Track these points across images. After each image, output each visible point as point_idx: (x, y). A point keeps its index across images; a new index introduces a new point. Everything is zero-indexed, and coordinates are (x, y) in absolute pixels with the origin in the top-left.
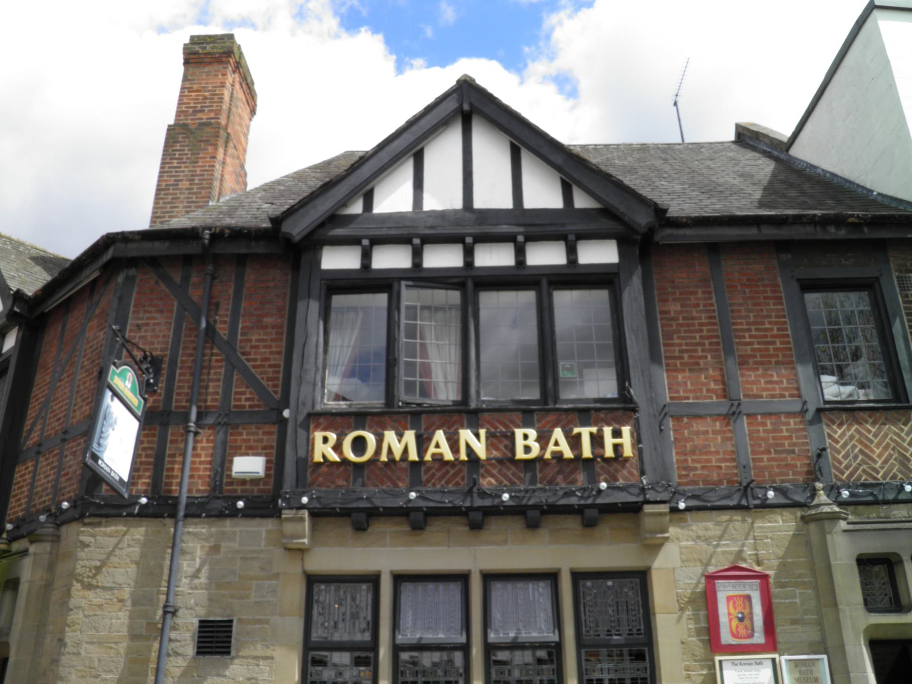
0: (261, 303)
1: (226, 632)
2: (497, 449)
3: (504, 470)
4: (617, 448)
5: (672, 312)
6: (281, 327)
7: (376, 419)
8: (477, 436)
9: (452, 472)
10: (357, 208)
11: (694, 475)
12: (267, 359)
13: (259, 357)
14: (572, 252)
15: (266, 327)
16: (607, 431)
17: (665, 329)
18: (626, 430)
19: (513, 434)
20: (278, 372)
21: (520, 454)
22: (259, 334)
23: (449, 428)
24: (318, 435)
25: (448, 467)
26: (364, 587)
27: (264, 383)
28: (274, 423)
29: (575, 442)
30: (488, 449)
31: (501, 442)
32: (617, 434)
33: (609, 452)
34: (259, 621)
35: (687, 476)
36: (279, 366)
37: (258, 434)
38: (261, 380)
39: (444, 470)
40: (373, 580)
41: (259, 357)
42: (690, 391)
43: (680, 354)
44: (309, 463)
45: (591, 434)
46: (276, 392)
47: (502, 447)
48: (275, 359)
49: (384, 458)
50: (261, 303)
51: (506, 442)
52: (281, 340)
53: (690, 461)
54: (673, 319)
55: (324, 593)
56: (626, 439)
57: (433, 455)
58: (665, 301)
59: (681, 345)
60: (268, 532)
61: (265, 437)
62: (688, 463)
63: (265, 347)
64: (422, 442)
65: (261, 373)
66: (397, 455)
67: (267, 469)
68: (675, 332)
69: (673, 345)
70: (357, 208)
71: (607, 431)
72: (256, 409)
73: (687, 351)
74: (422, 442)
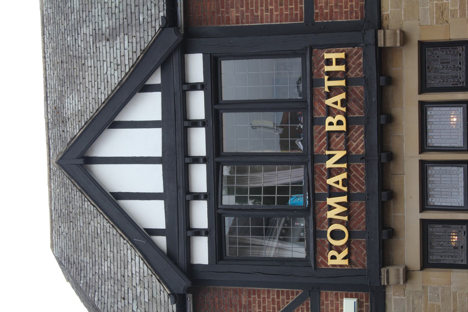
0: (231, 307)
1: (251, 179)
2: (338, 143)
3: (354, 138)
4: (339, 62)
5: (237, 15)
6: (249, 291)
7: (318, 224)
8: (330, 156)
9: (354, 173)
10: (162, 241)
11: (356, 8)
12: (273, 299)
13: (272, 306)
14: (194, 87)
15: (250, 302)
16: (327, 68)
17: (250, 20)
18: (327, 56)
19: (329, 132)
20: (283, 291)
21: (343, 128)
22: (255, 306)
23: (324, 174)
24: (331, 262)
25: (351, 176)
26: (430, 230)
27: (291, 301)
28: (320, 293)
29: (333, 91)
30: (340, 150)
31: (334, 140)
32: (329, 62)
33: (342, 68)
34: (455, 299)
35: (356, 12)
36: (278, 292)
37: (328, 304)
38: (289, 303)
39: (353, 178)
40: (424, 224)
41: (272, 306)
42: (296, 6)
43: (269, 11)
44: (349, 268)
45: (329, 80)
46: (297, 293)
47: (337, 140)
48: (273, 295)
49: (346, 218)
50: (231, 307)
51: (334, 136)
52: (260, 290)
53: (346, 10)
54: (243, 15)
55: (433, 258)
56: (333, 56)
57: (343, 185)
58: (228, 19)
59: (262, 10)
60: (394, 295)
61: (330, 299)
62: (348, 11)
63: (264, 302)
64: (332, 192)
65: (283, 304)
66: (343, 209)
67: (351, 297)
68: (252, 14)
69: (262, 16)
70: (162, 241)
71: (327, 68)
72: (310, 306)
73: (267, 6)
74: (332, 192)
